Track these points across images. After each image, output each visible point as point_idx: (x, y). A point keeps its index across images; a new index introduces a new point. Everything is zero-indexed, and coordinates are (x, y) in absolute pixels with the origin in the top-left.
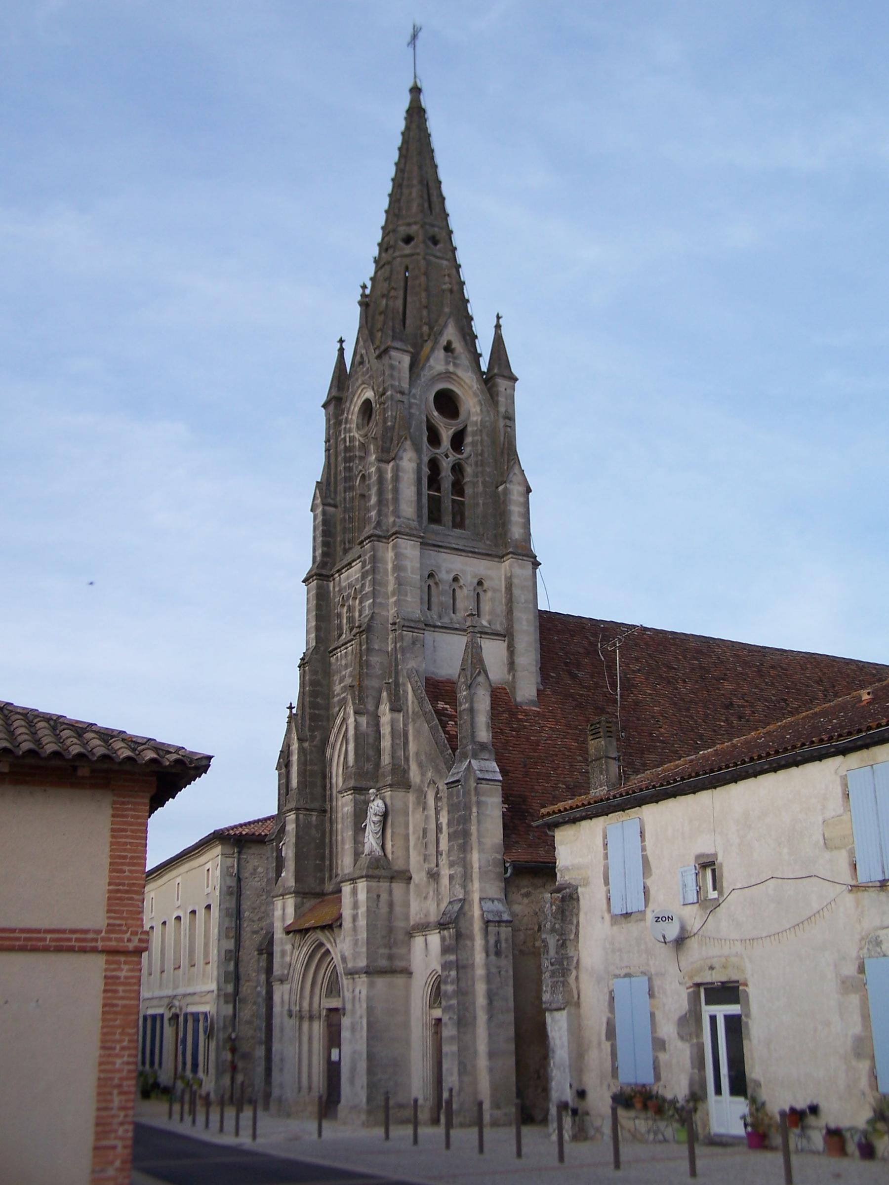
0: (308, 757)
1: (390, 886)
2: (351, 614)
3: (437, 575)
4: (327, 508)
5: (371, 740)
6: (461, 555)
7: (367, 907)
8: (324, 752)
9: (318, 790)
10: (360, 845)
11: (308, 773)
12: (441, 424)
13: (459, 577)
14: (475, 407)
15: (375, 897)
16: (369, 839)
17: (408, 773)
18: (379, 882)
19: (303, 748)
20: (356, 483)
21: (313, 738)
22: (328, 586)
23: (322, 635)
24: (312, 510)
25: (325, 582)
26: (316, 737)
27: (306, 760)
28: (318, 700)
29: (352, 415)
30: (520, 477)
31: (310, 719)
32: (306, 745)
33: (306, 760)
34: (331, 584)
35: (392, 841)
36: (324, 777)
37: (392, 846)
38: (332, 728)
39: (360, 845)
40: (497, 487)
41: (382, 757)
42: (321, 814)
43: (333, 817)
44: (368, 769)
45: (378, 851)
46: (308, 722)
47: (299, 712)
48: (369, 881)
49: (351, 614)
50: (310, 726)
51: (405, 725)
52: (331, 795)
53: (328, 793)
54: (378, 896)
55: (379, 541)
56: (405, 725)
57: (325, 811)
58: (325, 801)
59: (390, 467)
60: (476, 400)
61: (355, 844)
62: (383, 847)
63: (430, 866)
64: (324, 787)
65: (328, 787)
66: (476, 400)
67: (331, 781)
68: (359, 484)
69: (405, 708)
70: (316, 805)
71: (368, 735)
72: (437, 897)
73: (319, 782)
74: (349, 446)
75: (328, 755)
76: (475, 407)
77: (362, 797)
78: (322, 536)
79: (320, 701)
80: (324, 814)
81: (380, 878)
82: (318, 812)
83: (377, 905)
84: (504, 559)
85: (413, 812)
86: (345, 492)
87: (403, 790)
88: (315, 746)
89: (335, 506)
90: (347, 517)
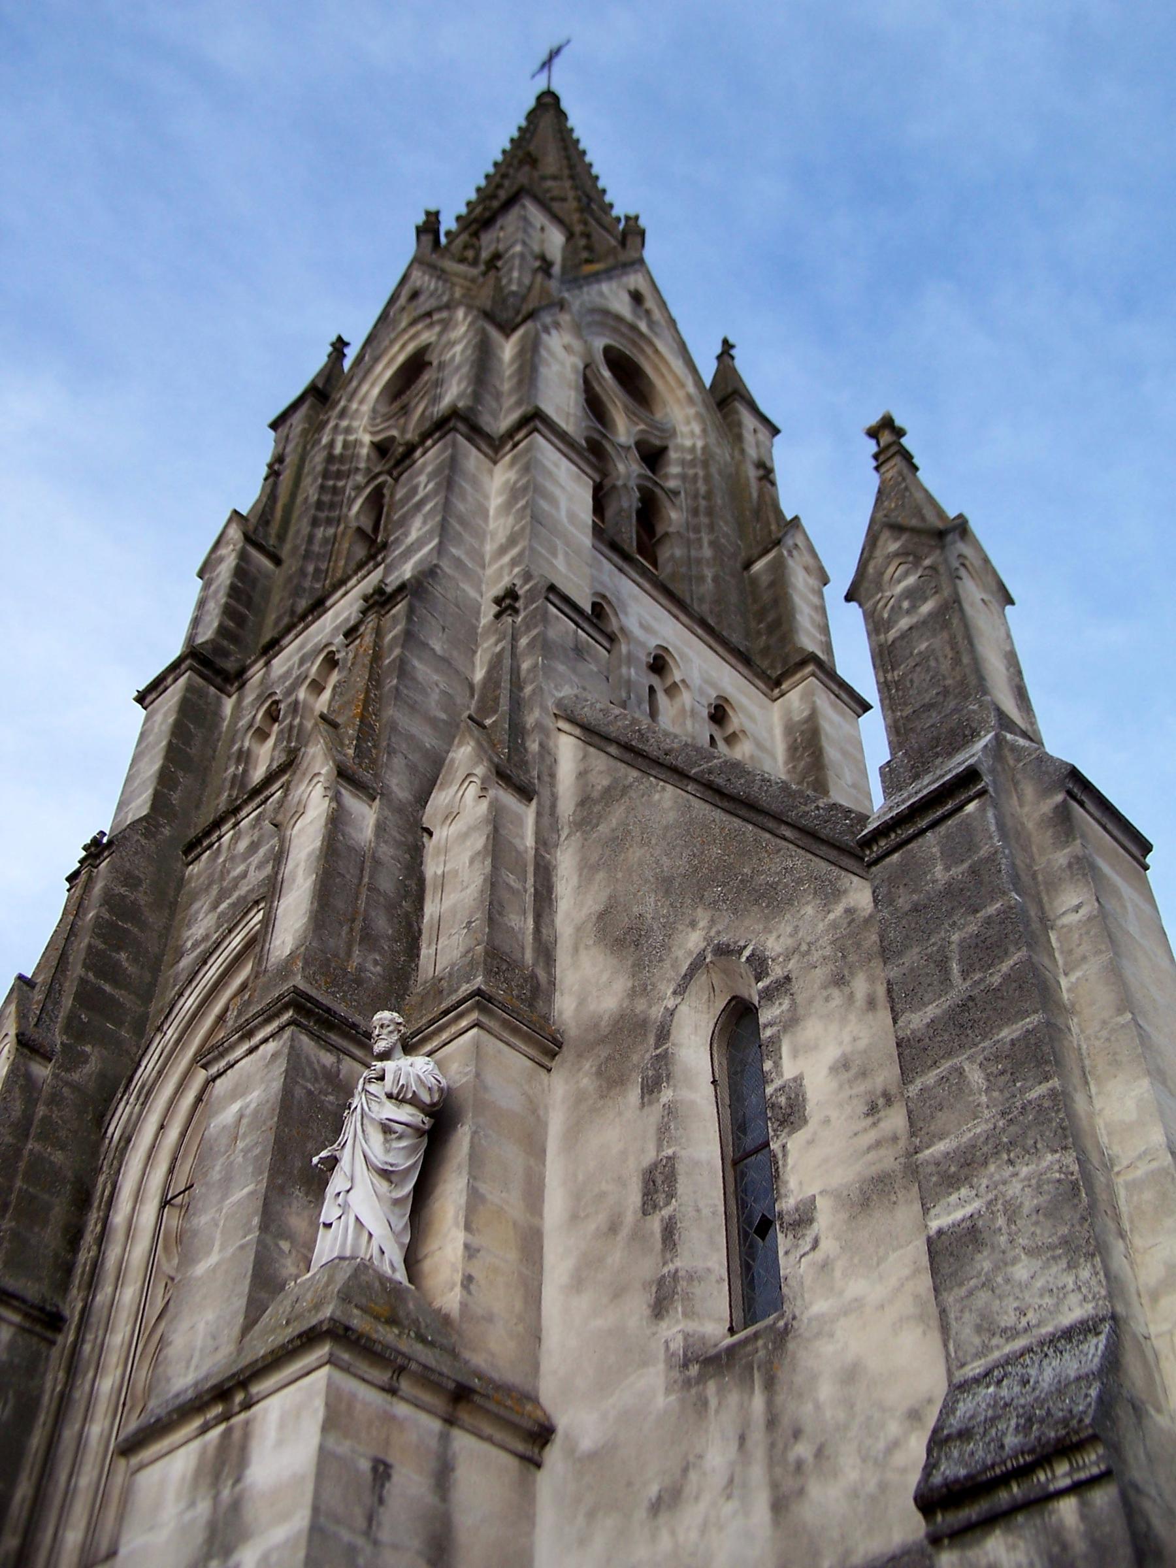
0: (41, 1111)
1: (444, 1438)
2: (297, 721)
3: (616, 614)
4: (254, 553)
5: (387, 883)
6: (677, 619)
7: (316, 1510)
8: (101, 1120)
9: (49, 1237)
10: (285, 1245)
11: (22, 1165)
12: (619, 404)
13: (668, 659)
14: (688, 423)
15: (365, 1465)
16: (345, 1207)
17: (550, 1001)
18: (392, 1391)
19: (28, 1076)
20: (349, 509)
21: (72, 1059)
22: (219, 704)
23: (175, 797)
24: (201, 575)
25: (212, 689)
26: (86, 1062)
27: (28, 1117)
28: (123, 956)
29: (361, 402)
30: (808, 559)
31: (78, 997)
32: (42, 1071)
33: (28, 1117)
34: (228, 705)
35: (468, 1228)
36: (82, 1199)
37: (470, 1251)
38: (159, 1029)
39: (285, 1245)
40: (748, 565)
41: (424, 952)
42: (38, 1328)
43: (87, 1348)
44: (361, 969)
45: (392, 1264)
46: (68, 1002)
47: (39, 980)
48: (346, 1369)
49: (297, 721)
50: (72, 1017)
51: (544, 843)
52: (97, 1265)
53: (84, 1256)
54: (382, 1471)
55: (469, 439)
56: (544, 843)
57: (54, 1321)
58: (63, 1287)
59: (508, 350)
60: (691, 411)
61: (264, 1227)
62: (412, 1259)
63: (691, 1326)
64: (74, 1238)
65: (89, 1238)
66: (691, 411)
67: (107, 1217)
68: (358, 513)
69: (545, 792)
70: (31, 1289)
71: (377, 862)
72: (775, 1456)
73: (59, 1209)
74: (341, 455)
75: (115, 1129)
76: (688, 423)
77: (328, 1059)
78: (229, 596)
79: (125, 964)
80: (49, 1334)
81: (400, 1370)
82: (26, 1315)
83: (370, 1518)
84: (783, 687)
85: (574, 1134)
86: (315, 523)
87: (531, 1052)
88: (74, 1087)
89: (277, 561)
90: (311, 569)
